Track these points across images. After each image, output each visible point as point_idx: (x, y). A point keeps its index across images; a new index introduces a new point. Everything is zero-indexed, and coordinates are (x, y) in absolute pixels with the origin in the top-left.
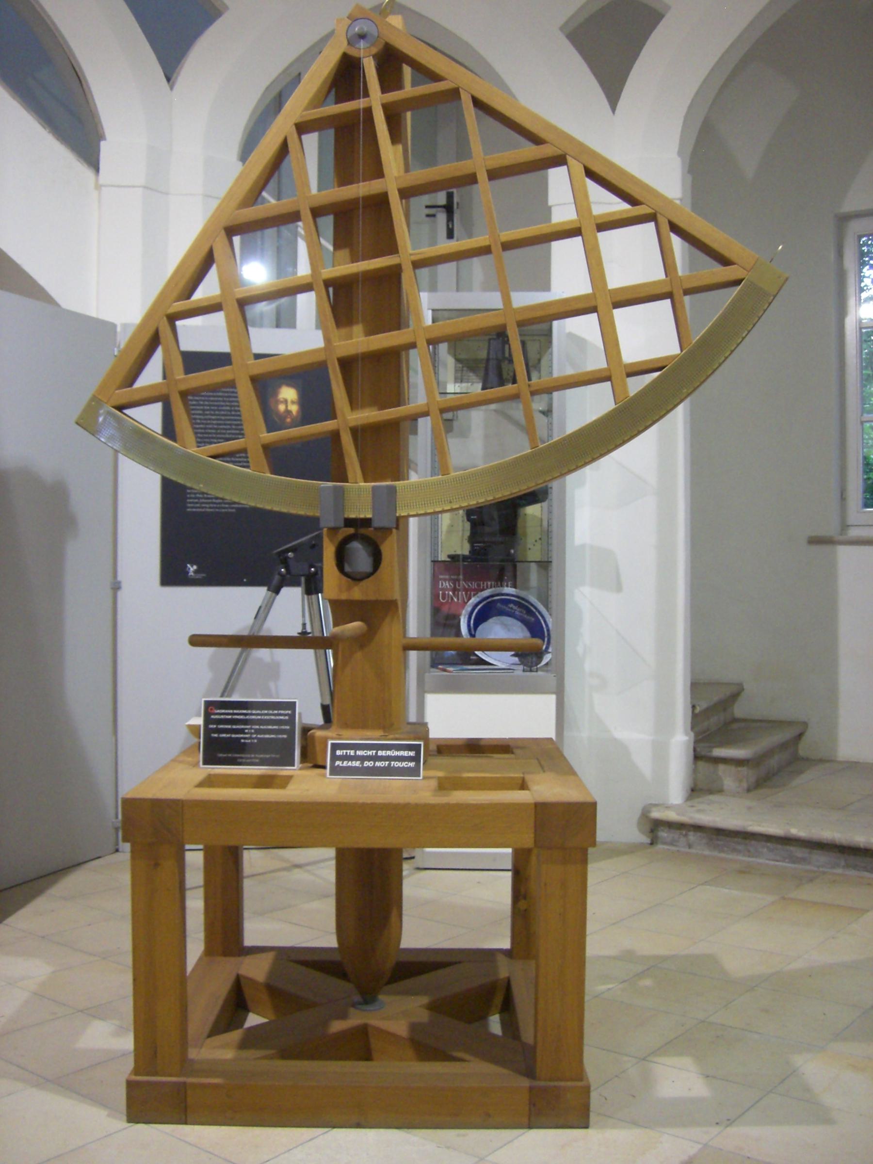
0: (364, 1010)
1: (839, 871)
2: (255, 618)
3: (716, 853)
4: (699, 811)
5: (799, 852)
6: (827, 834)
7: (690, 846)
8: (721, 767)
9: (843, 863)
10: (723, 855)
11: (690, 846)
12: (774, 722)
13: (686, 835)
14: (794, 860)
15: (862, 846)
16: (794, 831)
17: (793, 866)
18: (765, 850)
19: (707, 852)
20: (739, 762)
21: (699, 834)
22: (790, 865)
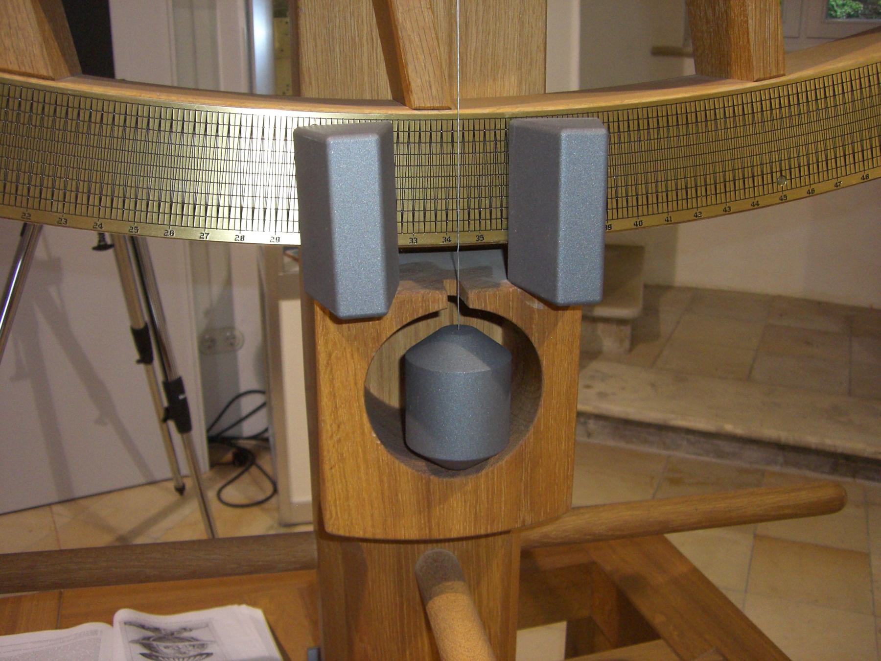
0: (41, 47)
1: (776, 468)
2: (23, 233)
3: (622, 444)
4: (602, 395)
5: (726, 446)
6: (770, 432)
7: (589, 435)
8: (600, 326)
9: (781, 459)
10: (630, 446)
11: (589, 435)
12: (299, 86)
13: (585, 424)
14: (720, 454)
15: (813, 446)
16: (729, 428)
17: (719, 461)
18: (685, 443)
19: (611, 443)
20: (621, 322)
21: (601, 422)
22: (714, 460)
